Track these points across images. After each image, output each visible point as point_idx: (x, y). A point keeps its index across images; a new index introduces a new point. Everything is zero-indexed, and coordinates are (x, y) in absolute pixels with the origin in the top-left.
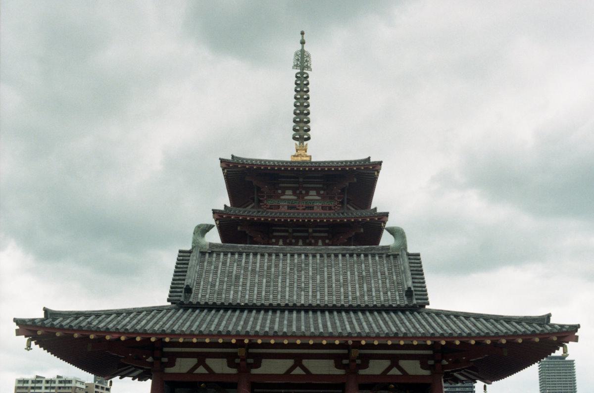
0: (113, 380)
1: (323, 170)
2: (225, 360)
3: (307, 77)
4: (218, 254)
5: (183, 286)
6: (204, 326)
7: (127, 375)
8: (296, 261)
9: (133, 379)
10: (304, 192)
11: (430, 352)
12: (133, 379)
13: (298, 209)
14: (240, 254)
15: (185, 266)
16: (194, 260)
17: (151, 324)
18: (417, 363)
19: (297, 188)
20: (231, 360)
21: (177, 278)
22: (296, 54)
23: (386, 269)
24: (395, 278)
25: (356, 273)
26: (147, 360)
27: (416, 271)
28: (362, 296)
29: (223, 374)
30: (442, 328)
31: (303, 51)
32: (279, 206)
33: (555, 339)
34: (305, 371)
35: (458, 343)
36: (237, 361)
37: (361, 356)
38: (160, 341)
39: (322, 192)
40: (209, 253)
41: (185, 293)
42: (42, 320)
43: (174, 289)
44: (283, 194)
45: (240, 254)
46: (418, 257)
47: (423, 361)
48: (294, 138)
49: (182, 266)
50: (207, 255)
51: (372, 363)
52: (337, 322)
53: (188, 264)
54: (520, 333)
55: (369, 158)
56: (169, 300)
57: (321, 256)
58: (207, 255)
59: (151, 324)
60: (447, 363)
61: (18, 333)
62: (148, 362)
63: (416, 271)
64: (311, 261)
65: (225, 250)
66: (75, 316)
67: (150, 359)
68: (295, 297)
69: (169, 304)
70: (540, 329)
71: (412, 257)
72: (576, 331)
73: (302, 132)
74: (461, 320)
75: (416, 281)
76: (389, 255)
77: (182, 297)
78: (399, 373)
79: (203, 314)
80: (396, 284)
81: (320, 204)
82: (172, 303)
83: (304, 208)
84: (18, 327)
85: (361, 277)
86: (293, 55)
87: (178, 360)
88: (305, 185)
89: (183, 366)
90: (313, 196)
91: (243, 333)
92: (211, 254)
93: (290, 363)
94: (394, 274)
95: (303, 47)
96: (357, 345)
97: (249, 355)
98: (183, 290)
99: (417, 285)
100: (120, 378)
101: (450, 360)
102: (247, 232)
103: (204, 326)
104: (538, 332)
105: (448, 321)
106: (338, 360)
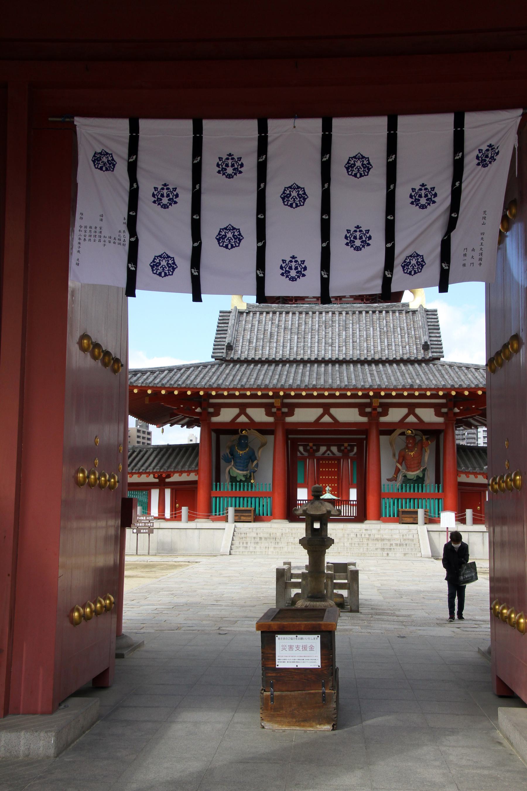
0: (164, 427)
4: (255, 313)
7: (176, 423)
9: (182, 427)
11: (443, 401)
12: (182, 427)
15: (226, 325)
20: (268, 408)
21: (219, 336)
23: (405, 324)
35: (466, 393)
36: (274, 410)
37: (382, 405)
41: (226, 350)
43: (217, 346)
45: (274, 313)
47: (437, 408)
49: (223, 325)
50: (245, 314)
53: (228, 323)
56: (212, 357)
57: (347, 313)
58: (245, 314)
64: (337, 318)
65: (260, 310)
66: (134, 373)
67: (198, 410)
68: (323, 352)
69: (214, 360)
75: (432, 335)
76: (409, 312)
77: (226, 356)
79: (243, 369)
80: (414, 339)
89: (226, 415)
91: (279, 386)
92: (248, 313)
94: (412, 329)
97: (284, 405)
98: (225, 347)
100: (171, 426)
101: (461, 408)
106: (361, 407)
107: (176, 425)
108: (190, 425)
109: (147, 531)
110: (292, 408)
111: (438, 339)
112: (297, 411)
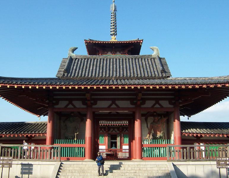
10: (115, 52)
18: (167, 102)
21: (61, 68)
26: (46, 102)
29: (167, 108)
34: (160, 106)
37: (142, 99)
46: (164, 59)
47: (170, 101)
51: (147, 102)
60: (181, 101)
78: (73, 107)
101: (183, 100)
106: (132, 101)
107: (46, 116)
109: (8, 166)
110: (95, 101)
111: (168, 69)
112: (99, 102)
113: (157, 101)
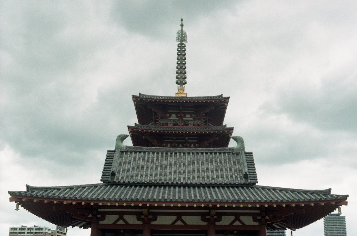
0: (68, 228)
1: (194, 102)
2: (135, 216)
3: (185, 46)
4: (131, 153)
5: (110, 172)
6: (123, 196)
7: (77, 225)
8: (178, 157)
9: (80, 228)
10: (182, 115)
11: (258, 211)
12: (80, 228)
13: (179, 126)
14: (144, 152)
15: (111, 160)
16: (116, 156)
17: (91, 194)
18: (251, 218)
19: (179, 113)
20: (139, 216)
21: (107, 167)
22: (178, 33)
23: (232, 162)
24: (237, 167)
25: (214, 164)
26: (88, 216)
27: (250, 162)
28: (218, 177)
29: (134, 225)
30: (265, 197)
31: (182, 31)
32: (168, 124)
33: (334, 203)
34: (183, 223)
35: (275, 206)
36: (143, 217)
37: (217, 214)
38: (96, 205)
39: (193, 115)
40: (126, 152)
41: (111, 176)
42: (25, 192)
43: (104, 174)
44: (170, 116)
45: (144, 152)
46: (251, 155)
47: (254, 217)
48: (177, 83)
49: (109, 160)
50: (125, 153)
51: (223, 218)
52: (203, 193)
53: (113, 159)
54: (313, 200)
55: (222, 95)
56: (101, 180)
57: (193, 154)
58: (125, 153)
59: (91, 194)
60: (269, 218)
61: (11, 200)
62: (89, 217)
63: (250, 162)
64: (187, 157)
65: (135, 150)
66: (45, 190)
67: (90, 216)
68: (177, 179)
69: (102, 182)
70: (325, 197)
71: (247, 154)
72: (346, 199)
73: (181, 79)
74: (277, 192)
75: (250, 168)
76: (234, 153)
77: (110, 178)
78: (240, 224)
79: (122, 188)
80: (238, 171)
81: (193, 123)
82: (103, 182)
83: (183, 125)
84: (11, 197)
85: (217, 166)
86: (176, 33)
87: (107, 216)
88: (183, 111)
89: (110, 220)
90: (188, 118)
91: (146, 200)
92: (127, 152)
93: (174, 218)
94: (237, 164)
95: (182, 28)
96: (214, 207)
97: (150, 213)
98: (110, 174)
99: (250, 171)
100: (72, 227)
101: (271, 216)
102: (148, 139)
103: (123, 196)
104: (323, 199)
105: (269, 193)
106: (203, 216)
108: (85, 227)
113: (121, 215)
